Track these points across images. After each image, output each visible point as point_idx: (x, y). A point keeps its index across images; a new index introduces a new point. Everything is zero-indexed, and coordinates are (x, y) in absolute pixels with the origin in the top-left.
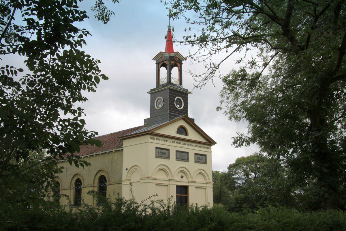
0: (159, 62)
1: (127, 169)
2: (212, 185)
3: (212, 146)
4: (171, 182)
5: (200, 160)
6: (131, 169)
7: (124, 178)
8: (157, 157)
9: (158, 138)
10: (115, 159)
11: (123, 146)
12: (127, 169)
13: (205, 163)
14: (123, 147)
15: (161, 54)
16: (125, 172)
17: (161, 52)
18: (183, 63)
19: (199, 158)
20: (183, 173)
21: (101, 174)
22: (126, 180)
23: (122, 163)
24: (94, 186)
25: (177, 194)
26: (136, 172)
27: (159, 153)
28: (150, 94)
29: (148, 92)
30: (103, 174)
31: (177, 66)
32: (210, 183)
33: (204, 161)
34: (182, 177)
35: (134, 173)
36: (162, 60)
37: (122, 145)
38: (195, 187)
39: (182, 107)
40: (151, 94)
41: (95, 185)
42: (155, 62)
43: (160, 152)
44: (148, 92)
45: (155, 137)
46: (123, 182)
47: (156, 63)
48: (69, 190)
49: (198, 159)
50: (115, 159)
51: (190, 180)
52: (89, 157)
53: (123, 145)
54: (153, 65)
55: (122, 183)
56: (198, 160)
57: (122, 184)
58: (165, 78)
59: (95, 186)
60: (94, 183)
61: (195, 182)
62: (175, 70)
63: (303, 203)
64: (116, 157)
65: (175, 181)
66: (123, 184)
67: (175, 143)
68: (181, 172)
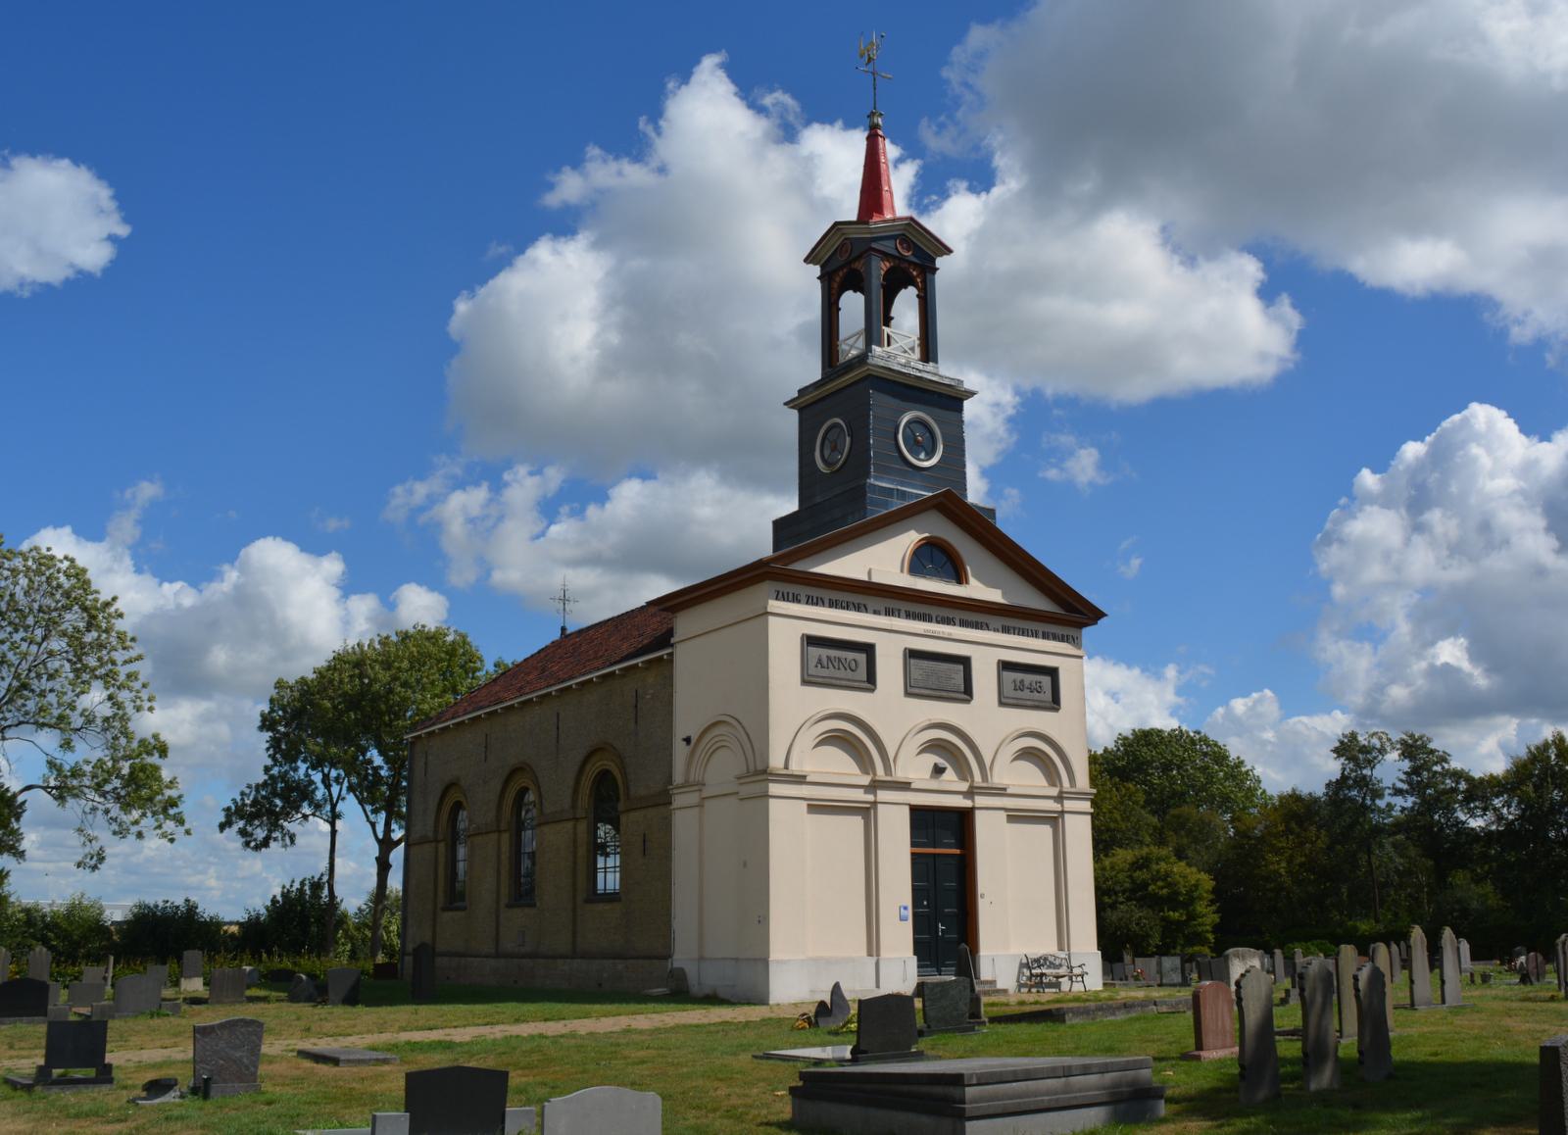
0: (829, 268)
1: (688, 740)
2: (1088, 804)
3: (1086, 631)
4: (883, 795)
5: (1026, 694)
6: (709, 736)
7: (678, 777)
8: (807, 681)
9: (815, 592)
10: (648, 697)
11: (672, 641)
12: (688, 740)
13: (1055, 703)
14: (672, 645)
15: (839, 233)
16: (680, 751)
17: (836, 224)
18: (937, 266)
19: (1022, 681)
20: (949, 750)
21: (598, 765)
22: (686, 784)
23: (670, 713)
24: (577, 819)
25: (913, 844)
26: (720, 753)
27: (820, 661)
28: (795, 413)
29: (786, 404)
30: (607, 767)
31: (915, 285)
32: (1079, 796)
33: (1048, 696)
34: (938, 771)
35: (716, 756)
36: (841, 259)
37: (670, 633)
38: (1004, 814)
39: (838, 420)
40: (801, 410)
41: (580, 813)
42: (816, 270)
43: (828, 658)
44: (786, 404)
45: (803, 591)
46: (677, 797)
47: (819, 274)
48: (496, 834)
49: (1020, 687)
50: (648, 697)
51: (881, 774)
52: (558, 697)
53: (672, 636)
54: (808, 282)
55: (671, 803)
56: (1019, 694)
57: (672, 807)
58: (858, 334)
59: (582, 818)
60: (574, 806)
61: (1001, 792)
62: (906, 307)
63: (92, 1006)
64: (651, 691)
65: (905, 786)
66: (674, 805)
67: (903, 613)
68: (939, 746)
